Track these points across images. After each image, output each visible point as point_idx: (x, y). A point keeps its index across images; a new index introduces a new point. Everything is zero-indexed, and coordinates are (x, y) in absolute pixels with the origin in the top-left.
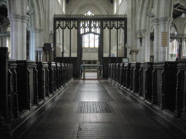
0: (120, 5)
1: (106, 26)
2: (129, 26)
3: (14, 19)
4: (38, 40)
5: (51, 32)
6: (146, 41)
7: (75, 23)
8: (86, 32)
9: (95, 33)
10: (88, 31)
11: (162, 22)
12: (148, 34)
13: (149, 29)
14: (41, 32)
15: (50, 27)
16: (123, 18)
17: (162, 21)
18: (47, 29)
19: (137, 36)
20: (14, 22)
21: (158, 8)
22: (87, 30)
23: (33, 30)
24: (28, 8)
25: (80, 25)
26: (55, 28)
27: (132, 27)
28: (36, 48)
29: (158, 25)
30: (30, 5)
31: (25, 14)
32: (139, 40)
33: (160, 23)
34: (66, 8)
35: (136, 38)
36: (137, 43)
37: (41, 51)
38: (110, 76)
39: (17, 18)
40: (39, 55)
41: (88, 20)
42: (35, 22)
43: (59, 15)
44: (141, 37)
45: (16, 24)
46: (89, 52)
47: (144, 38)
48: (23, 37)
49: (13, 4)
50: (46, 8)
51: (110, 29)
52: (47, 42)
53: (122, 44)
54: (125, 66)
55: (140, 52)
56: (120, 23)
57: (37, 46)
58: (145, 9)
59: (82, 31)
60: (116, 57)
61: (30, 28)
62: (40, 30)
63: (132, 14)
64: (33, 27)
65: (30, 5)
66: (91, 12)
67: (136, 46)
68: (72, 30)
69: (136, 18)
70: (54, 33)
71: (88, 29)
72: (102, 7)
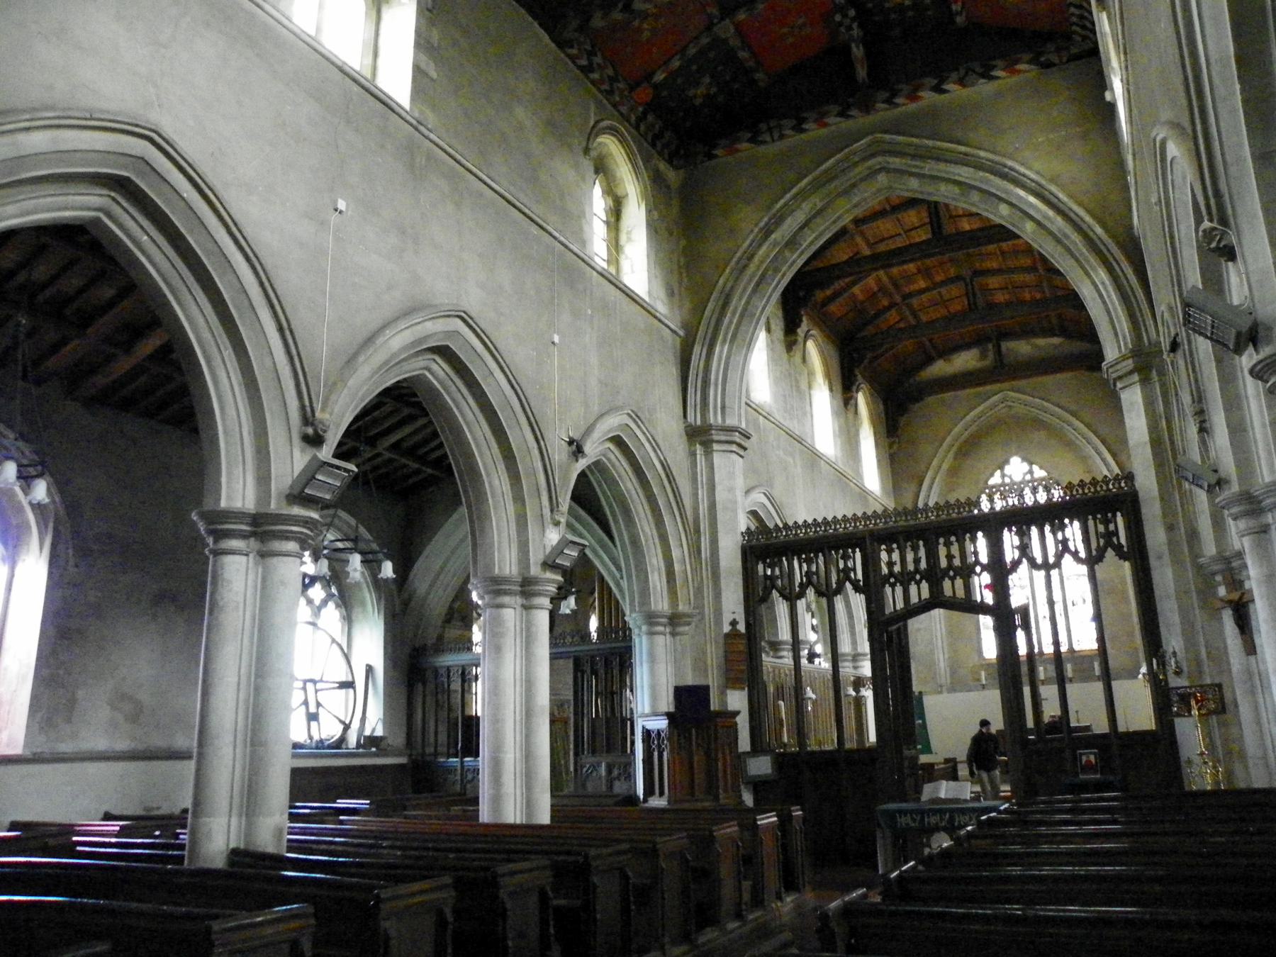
1: (1109, 544)
2: (1156, 536)
5: (734, 623)
8: (914, 599)
10: (926, 594)
14: (681, 629)
15: (724, 594)
16: (1116, 495)
18: (708, 611)
19: (1215, 594)
26: (756, 597)
27: (1172, 544)
31: (535, 570)
32: (1228, 617)
36: (1221, 633)
37: (663, 735)
39: (498, 593)
41: (979, 529)
43: (826, 522)
44: (1235, 596)
52: (690, 680)
54: (789, 737)
56: (1101, 528)
60: (1104, 736)
62: (675, 620)
66: (1024, 459)
67: (1219, 657)
68: (801, 604)
70: (748, 625)
71: (925, 586)
72: (1081, 426)
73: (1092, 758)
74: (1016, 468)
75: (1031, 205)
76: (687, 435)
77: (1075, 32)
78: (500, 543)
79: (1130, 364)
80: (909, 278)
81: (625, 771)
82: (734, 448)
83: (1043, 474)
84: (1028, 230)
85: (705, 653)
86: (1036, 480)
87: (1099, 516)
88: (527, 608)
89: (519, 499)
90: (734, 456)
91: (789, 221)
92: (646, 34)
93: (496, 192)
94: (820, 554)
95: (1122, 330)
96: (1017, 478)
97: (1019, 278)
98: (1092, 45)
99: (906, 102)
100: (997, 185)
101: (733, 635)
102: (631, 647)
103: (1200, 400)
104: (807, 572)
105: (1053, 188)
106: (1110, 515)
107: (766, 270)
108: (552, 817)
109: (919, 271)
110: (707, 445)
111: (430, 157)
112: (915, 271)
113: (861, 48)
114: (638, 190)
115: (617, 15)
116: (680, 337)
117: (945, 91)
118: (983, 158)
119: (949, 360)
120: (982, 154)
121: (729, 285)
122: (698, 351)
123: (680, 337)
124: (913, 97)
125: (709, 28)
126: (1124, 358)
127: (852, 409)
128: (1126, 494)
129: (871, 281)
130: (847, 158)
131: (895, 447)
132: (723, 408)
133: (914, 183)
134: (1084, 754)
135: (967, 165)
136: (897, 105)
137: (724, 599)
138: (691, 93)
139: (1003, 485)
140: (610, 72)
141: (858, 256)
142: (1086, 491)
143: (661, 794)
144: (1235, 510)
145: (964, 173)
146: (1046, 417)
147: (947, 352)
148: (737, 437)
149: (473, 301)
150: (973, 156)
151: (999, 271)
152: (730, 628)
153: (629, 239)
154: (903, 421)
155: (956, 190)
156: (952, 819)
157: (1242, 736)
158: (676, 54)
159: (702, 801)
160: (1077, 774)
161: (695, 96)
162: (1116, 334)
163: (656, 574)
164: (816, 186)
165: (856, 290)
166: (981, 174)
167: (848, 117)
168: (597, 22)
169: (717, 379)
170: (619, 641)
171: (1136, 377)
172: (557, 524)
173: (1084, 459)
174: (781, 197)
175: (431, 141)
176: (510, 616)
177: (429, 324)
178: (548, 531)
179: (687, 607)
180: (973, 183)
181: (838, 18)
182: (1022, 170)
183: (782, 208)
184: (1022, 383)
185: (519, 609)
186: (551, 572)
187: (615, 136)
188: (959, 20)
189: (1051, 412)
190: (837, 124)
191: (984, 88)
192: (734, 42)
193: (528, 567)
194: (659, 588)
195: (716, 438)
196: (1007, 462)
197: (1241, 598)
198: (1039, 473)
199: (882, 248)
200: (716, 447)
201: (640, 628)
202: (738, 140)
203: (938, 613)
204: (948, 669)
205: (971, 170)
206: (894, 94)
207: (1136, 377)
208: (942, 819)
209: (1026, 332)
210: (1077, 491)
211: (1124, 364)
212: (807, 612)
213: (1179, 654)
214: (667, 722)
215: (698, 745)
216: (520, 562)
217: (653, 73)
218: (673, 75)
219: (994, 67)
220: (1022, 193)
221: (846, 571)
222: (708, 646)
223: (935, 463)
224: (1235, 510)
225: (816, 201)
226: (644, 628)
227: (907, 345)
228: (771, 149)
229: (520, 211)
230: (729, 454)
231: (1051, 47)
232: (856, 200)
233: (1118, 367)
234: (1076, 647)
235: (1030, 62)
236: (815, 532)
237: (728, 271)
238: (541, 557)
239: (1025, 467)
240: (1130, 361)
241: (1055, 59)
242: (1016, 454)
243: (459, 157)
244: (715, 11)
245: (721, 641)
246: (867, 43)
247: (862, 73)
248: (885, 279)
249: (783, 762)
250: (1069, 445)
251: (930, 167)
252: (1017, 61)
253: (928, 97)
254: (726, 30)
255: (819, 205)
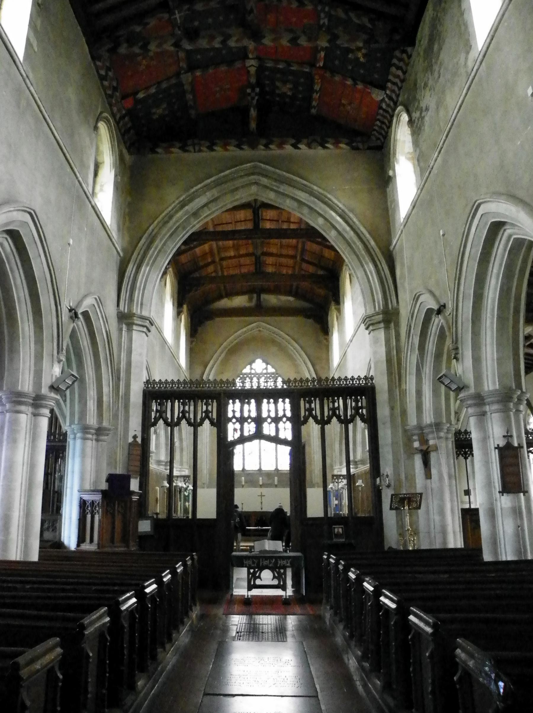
0: (351, 341)
1: (334, 414)
3: (8, 406)
4: (90, 464)
5: (135, 437)
6: (443, 461)
7: (210, 408)
8: (246, 434)
9: (276, 440)
11: (495, 407)
12: (447, 439)
13: (449, 421)
15: (131, 419)
17: (493, 403)
18: (120, 428)
20: (8, 415)
21: (477, 360)
22: (250, 428)
23: (75, 431)
24: (57, 370)
25: (226, 412)
27: (392, 415)
28: (82, 490)
29: (484, 414)
30: (64, 360)
31: (45, 390)
33: (487, 408)
34: (191, 352)
35: (410, 453)
36: (414, 469)
37: (96, 504)
38: (328, 598)
39: (20, 403)
40: (89, 516)
42: (85, 404)
43: (166, 382)
44: (424, 448)
45: (14, 423)
46: (261, 486)
47: (436, 449)
48: (32, 466)
49: (11, 360)
50: (119, 363)
51: (323, 422)
53: (363, 462)
55: (427, 499)
57: (87, 487)
58: (429, 359)
59: (232, 436)
61: (68, 423)
62: (100, 431)
63: (390, 373)
64: (76, 422)
65: (64, 360)
66: (264, 361)
67: (410, 478)
69: (403, 387)
70: (143, 439)
73: (340, 530)
74: (259, 366)
75: (337, 222)
76: (118, 318)
77: (374, 135)
78: (23, 370)
79: (380, 318)
80: (226, 249)
81: (53, 525)
82: (145, 330)
83: (273, 370)
84: (331, 236)
85: (116, 453)
86: (269, 374)
87: (353, 397)
88: (35, 415)
89: (39, 341)
90: (144, 334)
91: (197, 200)
92: (142, 67)
93: (55, 137)
94: (192, 401)
95: (378, 299)
96: (259, 371)
97: (283, 260)
98: (380, 144)
99: (276, 148)
100: (320, 207)
101: (134, 444)
102: (66, 446)
103: (456, 343)
104: (183, 410)
105: (351, 215)
106: (359, 397)
107: (178, 227)
108: (40, 556)
109: (234, 245)
110: (130, 326)
111: (29, 104)
112: (231, 245)
113: (256, 112)
114: (112, 162)
115: (136, 50)
116: (120, 256)
117: (299, 148)
118: (315, 190)
119: (231, 300)
120: (315, 188)
121: (155, 231)
122: (131, 269)
123: (120, 256)
124: (280, 146)
125: (178, 75)
126: (378, 314)
127: (179, 319)
128: (369, 387)
129: (206, 247)
130: (236, 172)
131: (194, 343)
132: (142, 304)
133: (272, 195)
134: (337, 528)
135: (306, 192)
136: (270, 149)
137: (130, 423)
138: (154, 110)
139: (250, 374)
140: (115, 84)
141: (207, 230)
142: (297, 385)
143: (92, 541)
144: (469, 402)
145: (302, 196)
146: (279, 339)
147: (230, 295)
148: (147, 323)
149: (37, 205)
150: (309, 187)
151: (276, 255)
152: (133, 440)
153: (101, 190)
154: (200, 329)
155: (295, 204)
156: (276, 563)
157: (418, 521)
158: (154, 85)
159: (118, 547)
160: (332, 539)
161: (154, 113)
162: (374, 301)
163: (92, 401)
164: (218, 184)
165: (198, 250)
166: (312, 198)
167: (242, 149)
168: (123, 50)
169: (140, 286)
170: (56, 442)
171: (382, 325)
172: (59, 361)
173: (296, 366)
174: (196, 185)
175: (30, 91)
176: (24, 419)
177: (15, 213)
178: (55, 366)
179: (108, 424)
180: (306, 202)
181: (249, 91)
182: (336, 201)
183: (194, 192)
184: (268, 319)
185: (30, 415)
186: (54, 393)
187: (107, 124)
188: (313, 111)
189: (282, 336)
190: (233, 151)
191: (320, 151)
192: (187, 87)
193: (40, 387)
194: (92, 410)
195: (136, 322)
196: (254, 361)
197: (428, 449)
198: (271, 370)
199: (220, 229)
200: (135, 327)
201: (75, 434)
202: (173, 146)
203: (256, 442)
204: (208, 475)
205: (307, 195)
206: (271, 142)
207: (382, 325)
208: (270, 563)
209: (276, 291)
210: (349, 382)
211: (377, 317)
212: (154, 434)
213: (389, 475)
214: (101, 496)
215: (119, 512)
216: (35, 383)
217: (137, 93)
218: (149, 97)
219: (327, 142)
220: (334, 214)
221: (334, 410)
222: (118, 449)
223: (215, 356)
224: (469, 402)
225: (215, 193)
226: (79, 435)
227: (209, 287)
228: (191, 156)
229: (64, 154)
230: (141, 333)
231: (359, 139)
232: (237, 197)
233: (373, 318)
234: (247, 468)
235: (347, 144)
236: (178, 387)
237: (156, 222)
238: (49, 384)
239: (264, 365)
240: (381, 316)
241: (360, 146)
242: (260, 358)
243: (42, 108)
244: (183, 65)
245: (126, 447)
246: (260, 108)
247: (253, 125)
248: (215, 246)
249: (157, 523)
250: (290, 358)
251: (284, 188)
252: (340, 142)
253: (288, 148)
254: (187, 78)
255: (216, 195)
